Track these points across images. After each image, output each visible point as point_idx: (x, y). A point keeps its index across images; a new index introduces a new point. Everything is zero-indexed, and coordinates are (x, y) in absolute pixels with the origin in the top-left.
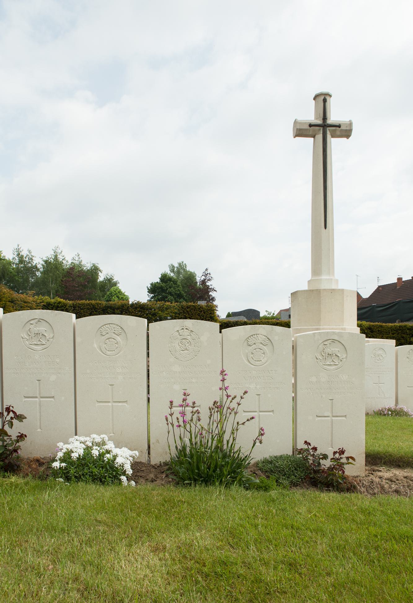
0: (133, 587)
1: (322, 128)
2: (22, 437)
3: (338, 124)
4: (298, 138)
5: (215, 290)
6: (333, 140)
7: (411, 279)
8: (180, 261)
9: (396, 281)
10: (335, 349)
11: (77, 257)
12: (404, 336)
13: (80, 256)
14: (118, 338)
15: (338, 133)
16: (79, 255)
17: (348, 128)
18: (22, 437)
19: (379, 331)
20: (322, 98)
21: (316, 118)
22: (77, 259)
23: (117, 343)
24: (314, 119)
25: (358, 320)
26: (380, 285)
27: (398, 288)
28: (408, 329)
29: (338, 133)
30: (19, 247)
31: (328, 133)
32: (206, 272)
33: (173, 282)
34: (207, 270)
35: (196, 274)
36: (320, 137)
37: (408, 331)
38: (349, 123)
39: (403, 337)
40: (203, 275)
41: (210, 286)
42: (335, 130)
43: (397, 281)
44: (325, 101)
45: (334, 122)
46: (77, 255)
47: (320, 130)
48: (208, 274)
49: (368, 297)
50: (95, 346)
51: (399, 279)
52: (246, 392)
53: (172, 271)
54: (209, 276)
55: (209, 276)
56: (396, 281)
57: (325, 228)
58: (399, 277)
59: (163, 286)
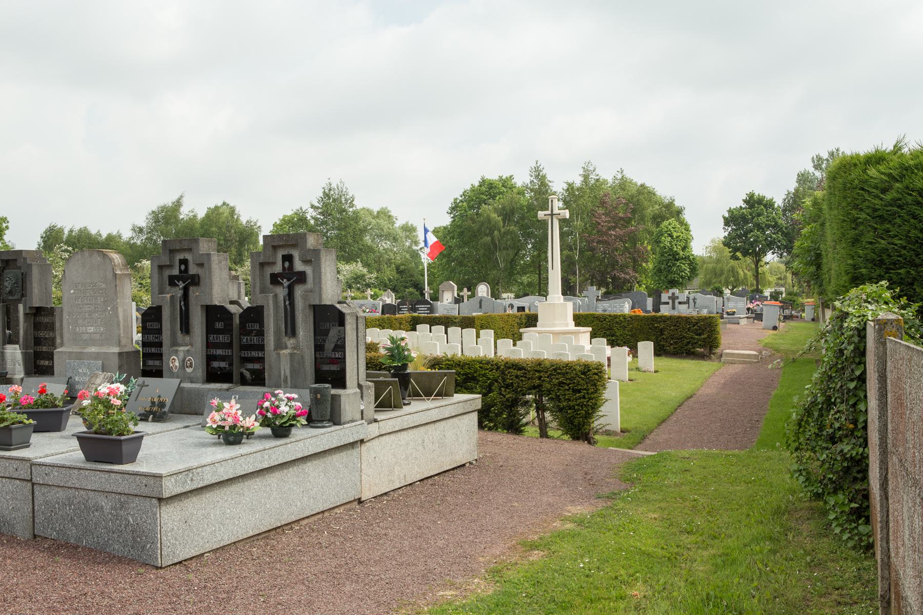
0: (498, 587)
2: (313, 207)
8: (832, 148)
13: (624, 173)
18: (313, 207)
25: (162, 370)
30: (538, 165)
33: (765, 206)
53: (817, 167)
56: (418, 326)
59: (746, 213)
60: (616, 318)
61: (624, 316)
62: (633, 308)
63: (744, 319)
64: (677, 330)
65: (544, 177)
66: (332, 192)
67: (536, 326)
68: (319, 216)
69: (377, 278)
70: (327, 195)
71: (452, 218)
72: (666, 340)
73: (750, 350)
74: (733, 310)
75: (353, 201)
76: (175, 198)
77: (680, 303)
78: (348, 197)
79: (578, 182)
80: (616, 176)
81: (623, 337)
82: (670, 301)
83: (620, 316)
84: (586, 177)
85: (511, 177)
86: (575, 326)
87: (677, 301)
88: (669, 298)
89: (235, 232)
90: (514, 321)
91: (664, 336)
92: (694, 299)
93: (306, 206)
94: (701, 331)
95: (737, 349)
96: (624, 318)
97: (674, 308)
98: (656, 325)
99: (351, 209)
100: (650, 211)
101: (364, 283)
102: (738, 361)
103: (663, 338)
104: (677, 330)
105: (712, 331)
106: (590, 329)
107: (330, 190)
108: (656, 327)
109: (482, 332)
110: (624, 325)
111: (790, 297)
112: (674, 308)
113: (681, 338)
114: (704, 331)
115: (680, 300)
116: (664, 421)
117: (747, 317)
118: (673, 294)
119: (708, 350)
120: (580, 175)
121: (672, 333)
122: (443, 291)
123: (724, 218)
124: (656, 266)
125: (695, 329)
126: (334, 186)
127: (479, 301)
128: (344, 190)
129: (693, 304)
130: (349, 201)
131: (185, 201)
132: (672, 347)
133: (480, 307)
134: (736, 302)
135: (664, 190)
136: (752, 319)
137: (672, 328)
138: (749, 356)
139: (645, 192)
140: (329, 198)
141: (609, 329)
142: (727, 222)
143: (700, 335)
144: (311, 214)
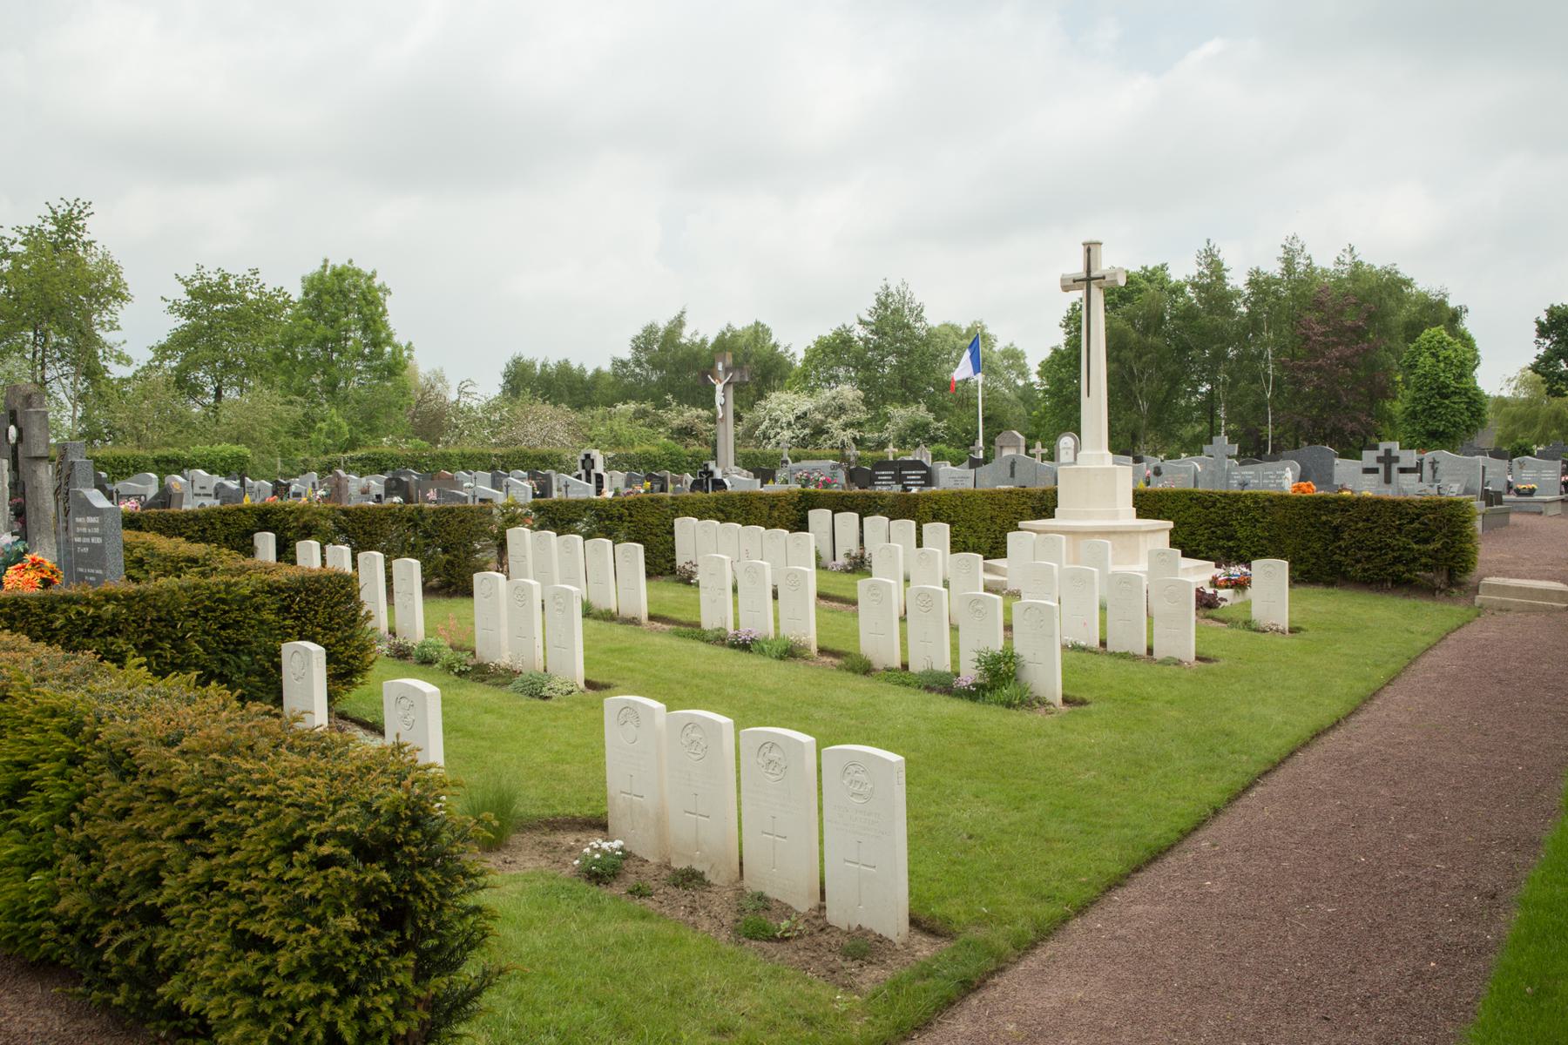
2: (861, 322)
11: (1347, 255)
13: (1356, 252)
16: (1352, 249)
18: (861, 322)
22: (1348, 260)
30: (1211, 246)
31: (1092, 286)
43: (1005, 537)
46: (1348, 250)
60: (1237, 501)
61: (1283, 499)
62: (1302, 478)
63: (1554, 505)
64: (1371, 529)
65: (1220, 264)
66: (890, 300)
67: (1054, 517)
68: (870, 336)
69: (948, 428)
70: (883, 304)
71: (1067, 333)
72: (1345, 551)
73: (1549, 579)
74: (1531, 486)
75: (922, 310)
76: (672, 314)
77: (1403, 470)
78: (914, 305)
79: (1274, 269)
80: (1342, 259)
81: (1252, 542)
82: (1381, 467)
83: (1246, 496)
84: (1289, 263)
85: (1163, 266)
86: (1138, 516)
87: (1395, 467)
88: (1379, 460)
89: (756, 363)
90: (1025, 503)
91: (1341, 543)
92: (1434, 463)
93: (851, 322)
94: (1428, 534)
95: (1517, 577)
96: (1256, 502)
97: (1388, 480)
98: (1324, 518)
99: (918, 325)
100: (1403, 315)
101: (927, 436)
102: (1517, 604)
103: (1340, 547)
104: (1371, 529)
105: (1454, 534)
106: (1170, 524)
107: (887, 296)
108: (1325, 523)
109: (927, 528)
110: (1254, 517)
111: (482, 504)
112: (1388, 480)
113: (1381, 549)
114: (1434, 533)
115: (1402, 464)
116: (1157, 855)
117: (1562, 500)
118: (1388, 451)
119: (1444, 578)
120: (1279, 259)
121: (1360, 536)
122: (1002, 447)
123: (1538, 322)
124: (1407, 408)
125: (1415, 529)
126: (893, 289)
127: (1009, 463)
128: (908, 296)
129: (1431, 472)
130: (916, 312)
131: (687, 318)
132: (1359, 566)
133: (1012, 475)
134: (1539, 470)
135: (1426, 281)
136: (489, 884)
137: (1360, 525)
138: (1546, 594)
139: (1394, 286)
140: (886, 309)
141: (1222, 525)
142: (1543, 331)
143: (1426, 541)
144: (859, 332)
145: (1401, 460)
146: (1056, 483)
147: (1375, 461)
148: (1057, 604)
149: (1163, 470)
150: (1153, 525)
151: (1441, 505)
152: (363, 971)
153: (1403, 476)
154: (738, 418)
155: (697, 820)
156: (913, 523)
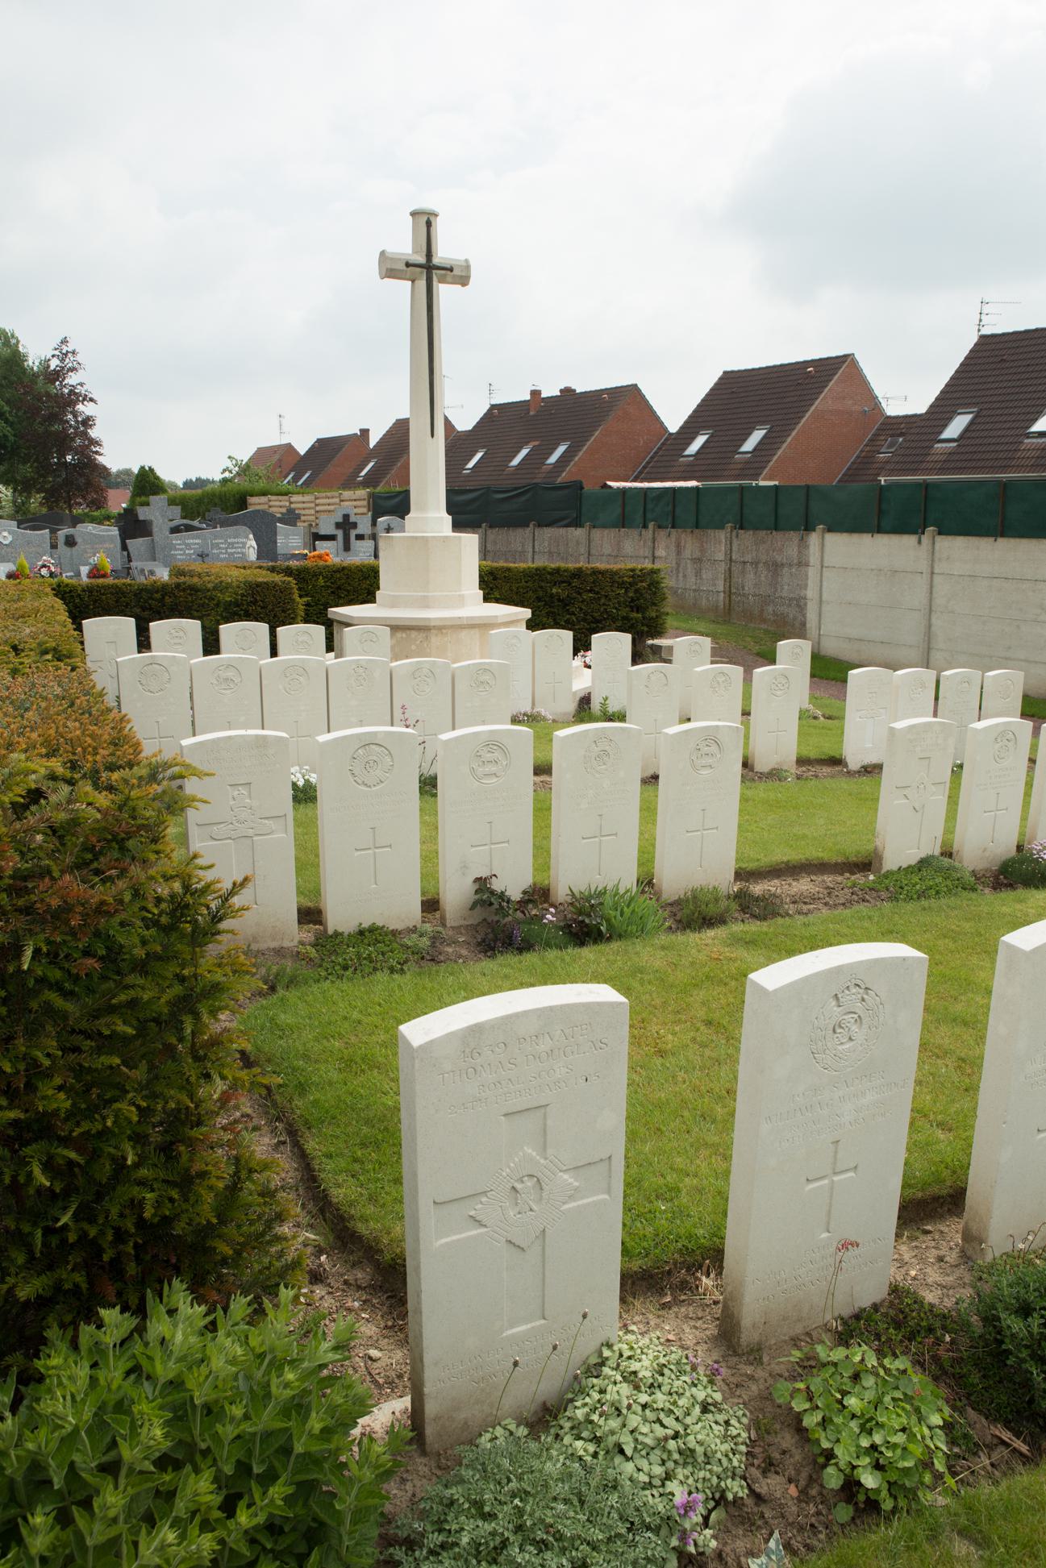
1: (425, 271)
3: (449, 266)
4: (387, 280)
5: (91, 400)
6: (441, 286)
7: (559, 394)
9: (528, 397)
10: (486, 677)
12: (543, 584)
14: (301, 679)
15: (449, 279)
17: (463, 274)
19: (505, 577)
20: (425, 219)
21: (415, 251)
23: (300, 683)
24: (410, 252)
26: (494, 403)
27: (532, 413)
28: (549, 573)
29: (449, 279)
32: (64, 346)
34: (64, 341)
35: (17, 338)
36: (422, 284)
37: (549, 577)
38: (464, 264)
39: (541, 587)
40: (53, 356)
41: (79, 387)
42: (445, 275)
44: (429, 224)
45: (443, 261)
47: (422, 273)
48: (70, 355)
49: (470, 427)
50: (281, 687)
51: (535, 393)
52: (417, 721)
54: (72, 359)
55: (72, 359)
56: (528, 397)
57: (432, 436)
58: (534, 388)
82: (340, 534)
86: (486, 599)
87: (353, 533)
97: (347, 547)
109: (159, 629)
112: (347, 547)
145: (359, 526)
146: (376, 556)
147: (333, 527)
148: (736, 723)
149: (79, 540)
150: (516, 614)
151: (344, 568)
152: (172, 914)
153: (359, 543)
154: (294, 1237)
155: (375, 853)
156: (131, 622)
